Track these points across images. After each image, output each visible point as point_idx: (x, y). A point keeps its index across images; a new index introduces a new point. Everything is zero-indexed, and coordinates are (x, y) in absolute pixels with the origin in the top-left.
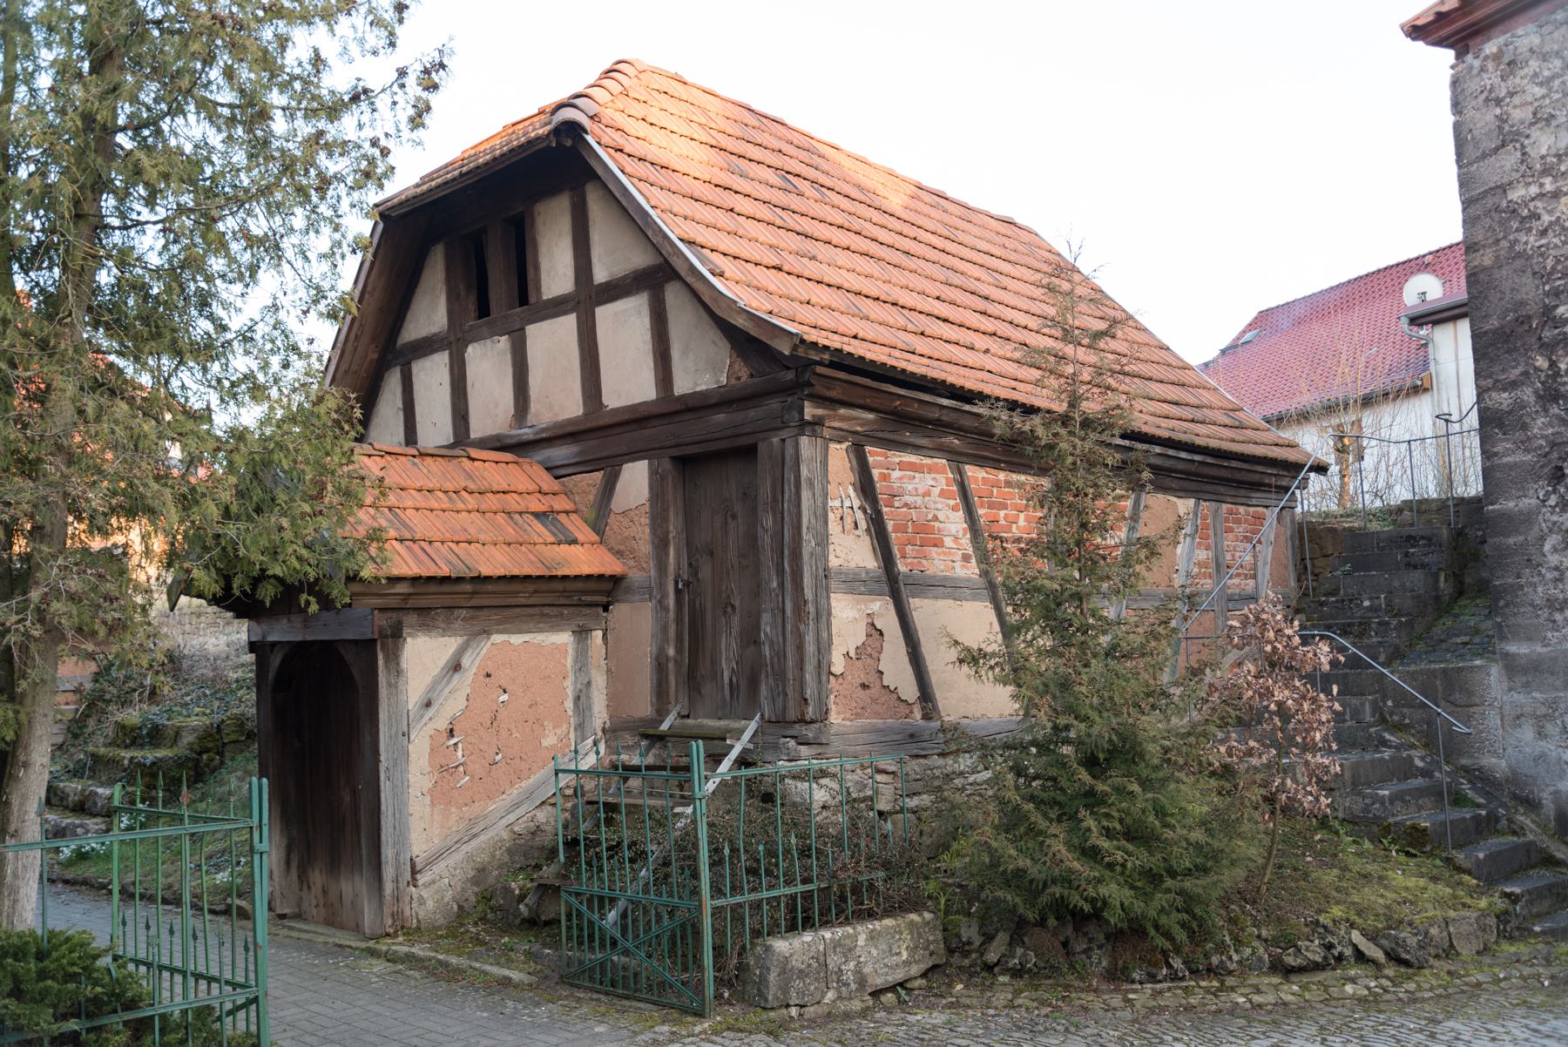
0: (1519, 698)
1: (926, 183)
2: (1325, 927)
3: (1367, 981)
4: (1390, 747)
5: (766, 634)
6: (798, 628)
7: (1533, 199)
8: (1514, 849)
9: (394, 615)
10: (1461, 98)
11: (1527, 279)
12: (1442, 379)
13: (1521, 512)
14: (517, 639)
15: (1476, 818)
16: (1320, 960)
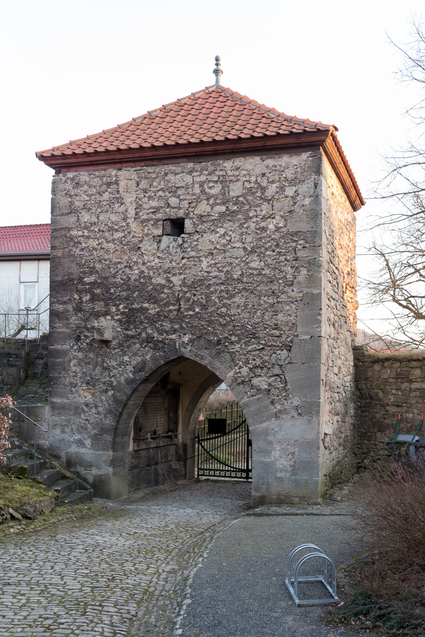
0: (56, 418)
7: (80, 237)
10: (56, 189)
11: (74, 265)
13: (63, 350)
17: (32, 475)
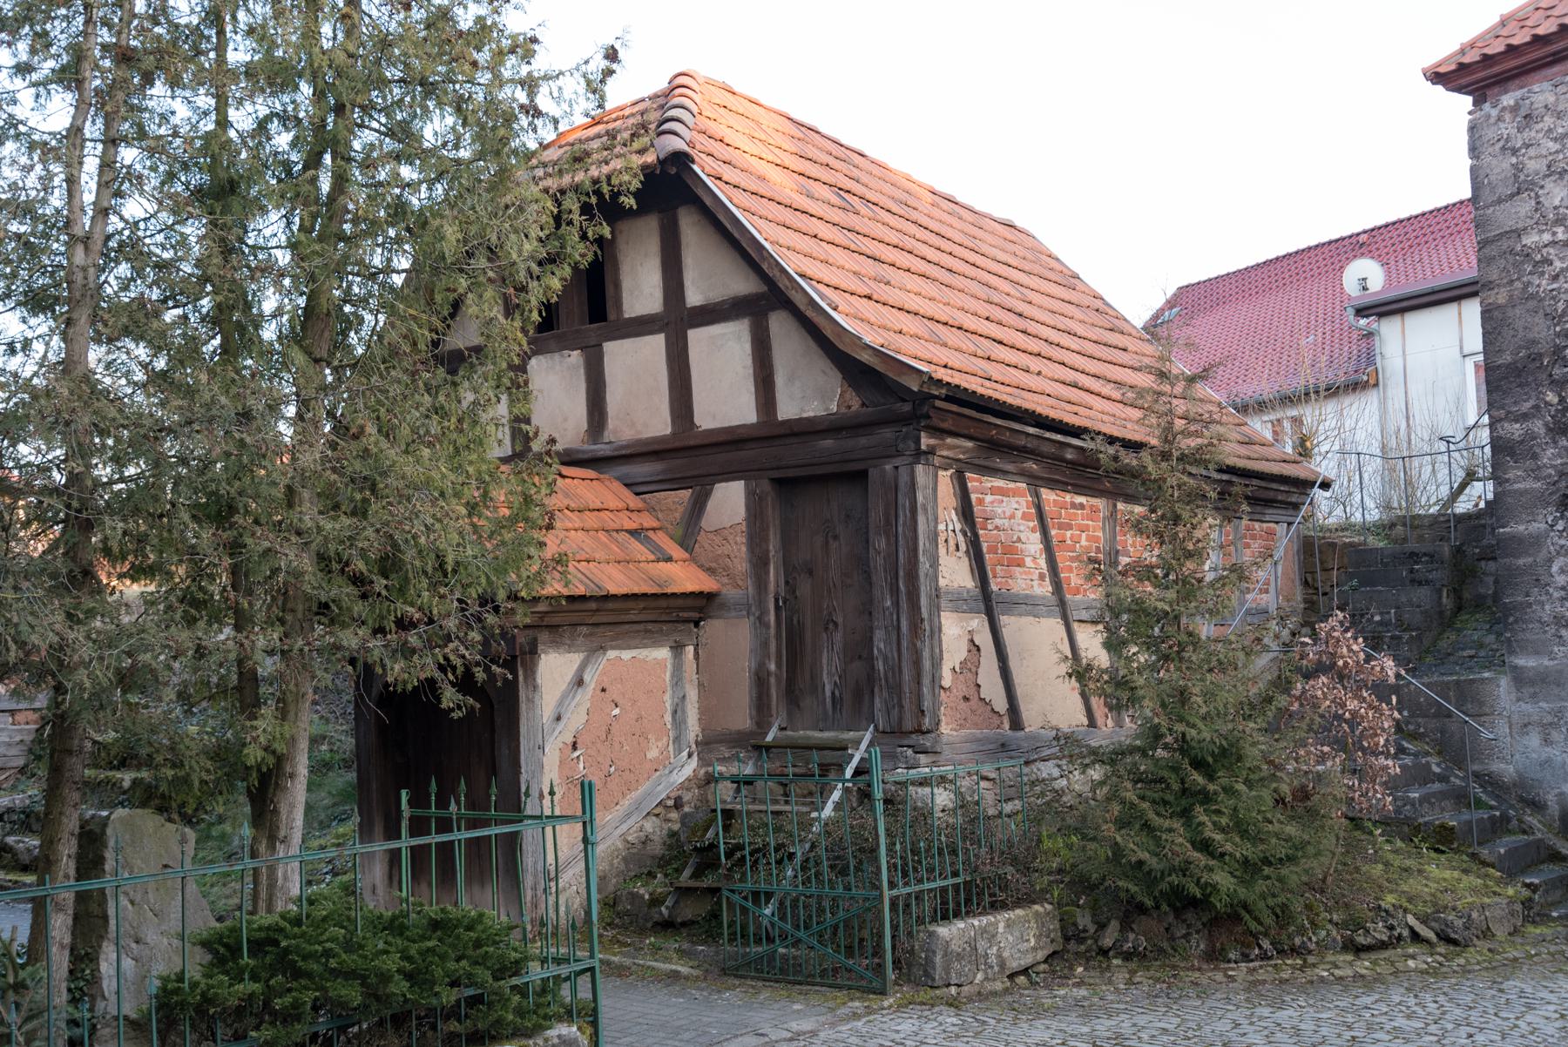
0: (1527, 707)
1: (939, 188)
2: (1386, 911)
3: (1424, 958)
4: (1409, 754)
5: (879, 650)
6: (915, 645)
7: (1546, 246)
8: (1528, 845)
9: (530, 632)
10: (1478, 143)
11: (1539, 319)
12: (1388, 374)
14: (626, 655)
15: (1492, 818)
16: (1386, 939)
17: (1470, 846)
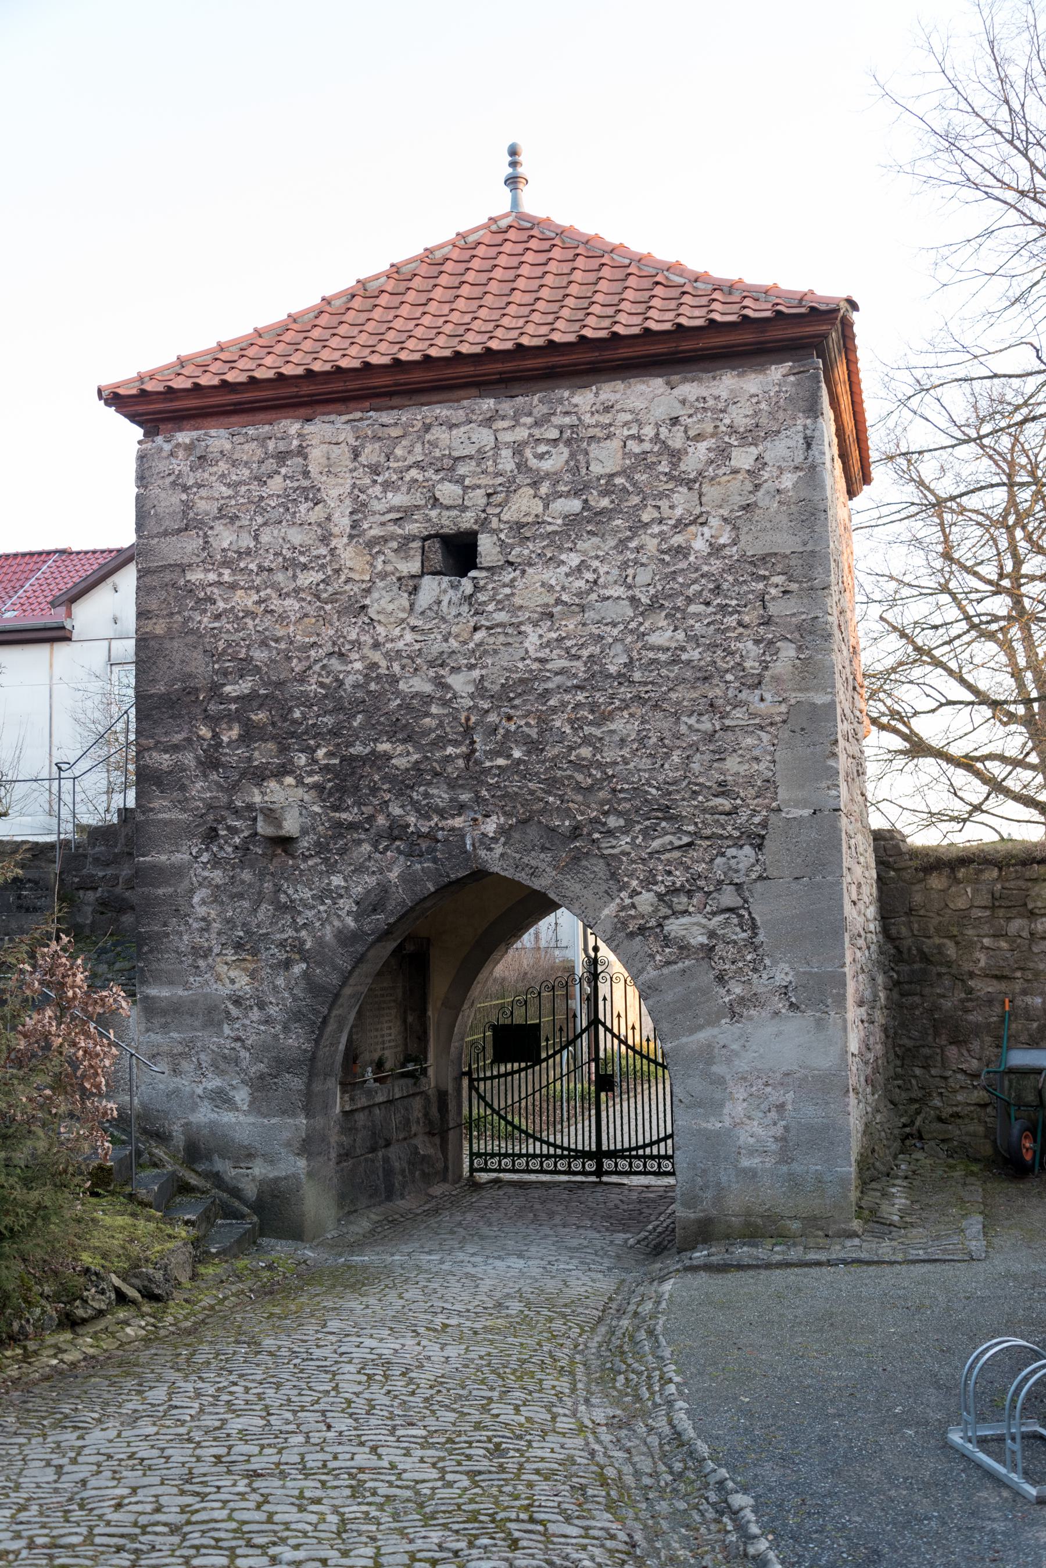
0: (156, 1038)
2: (96, 1274)
7: (210, 585)
10: (147, 474)
11: (198, 655)
